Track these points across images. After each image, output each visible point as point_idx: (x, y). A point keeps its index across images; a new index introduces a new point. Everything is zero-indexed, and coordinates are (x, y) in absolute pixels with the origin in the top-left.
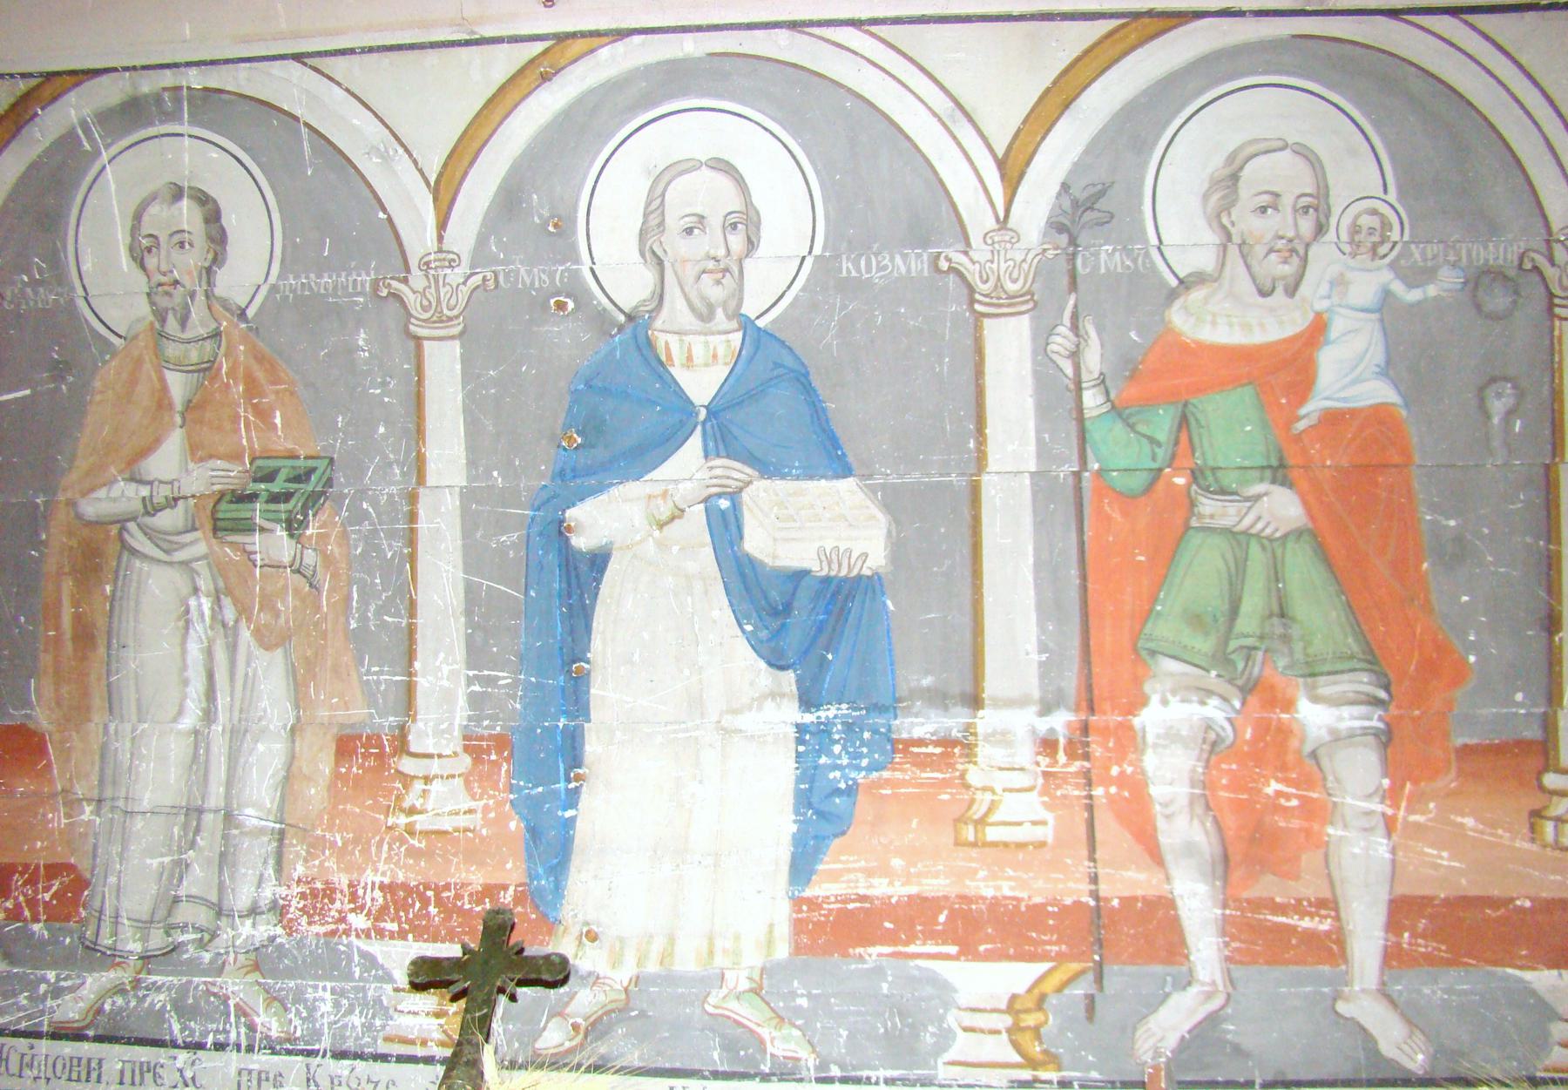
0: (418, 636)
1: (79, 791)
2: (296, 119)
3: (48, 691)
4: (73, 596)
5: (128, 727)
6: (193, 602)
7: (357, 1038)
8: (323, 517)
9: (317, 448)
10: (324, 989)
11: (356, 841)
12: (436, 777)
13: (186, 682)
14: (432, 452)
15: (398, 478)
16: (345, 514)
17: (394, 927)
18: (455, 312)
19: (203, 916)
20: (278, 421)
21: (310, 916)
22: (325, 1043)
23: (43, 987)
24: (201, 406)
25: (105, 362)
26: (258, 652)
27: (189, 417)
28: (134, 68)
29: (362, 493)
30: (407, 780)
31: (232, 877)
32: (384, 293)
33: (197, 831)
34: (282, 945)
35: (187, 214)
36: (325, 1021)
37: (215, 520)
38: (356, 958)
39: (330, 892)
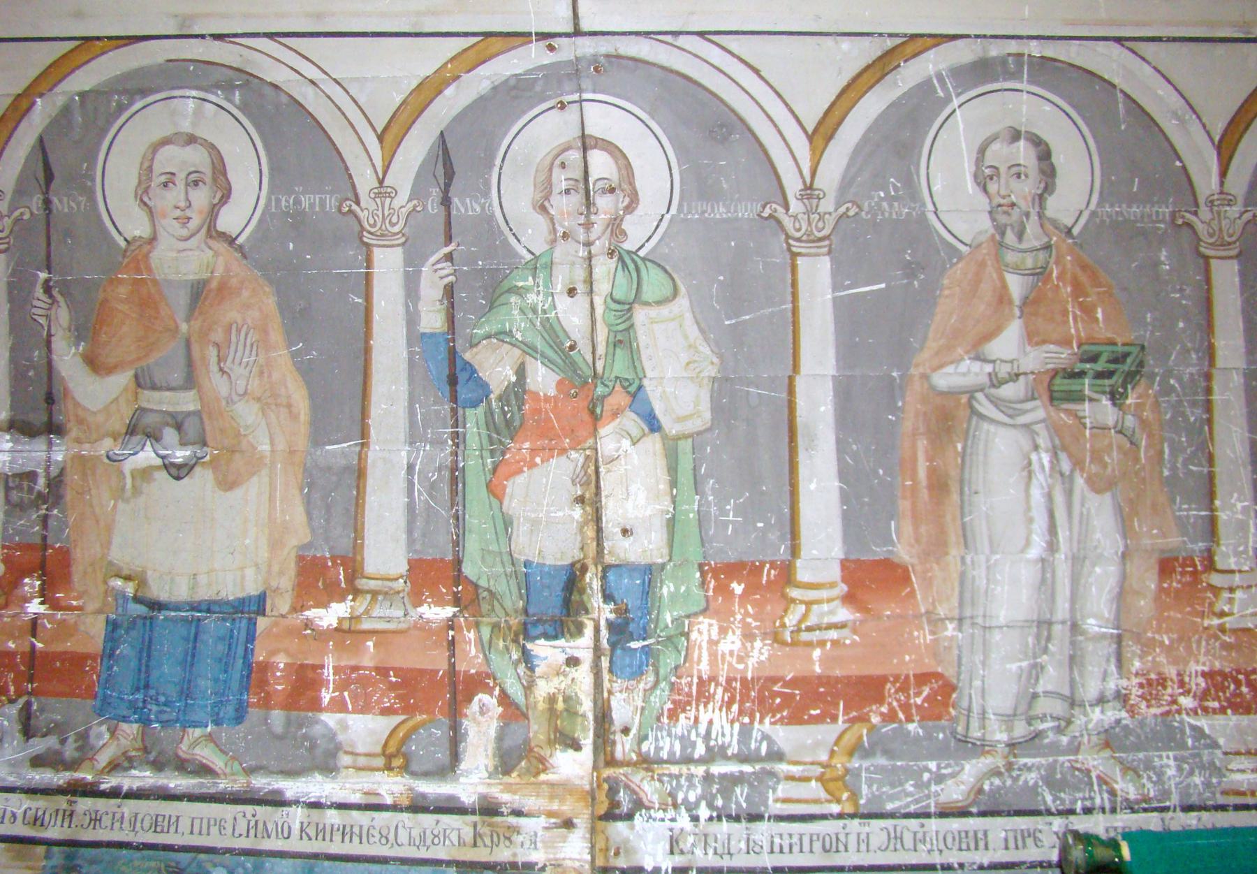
0: (1217, 481)
1: (941, 611)
2: (1114, 86)
3: (908, 528)
4: (926, 452)
5: (982, 558)
6: (1034, 457)
7: (1200, 794)
8: (1140, 389)
9: (1132, 337)
10: (1168, 757)
11: (1180, 639)
12: (1238, 587)
13: (1031, 520)
14: (1220, 343)
15: (1195, 361)
16: (1156, 387)
17: (1216, 704)
18: (1234, 239)
19: (1059, 708)
20: (1100, 315)
21: (1148, 701)
22: (1174, 799)
23: (926, 776)
24: (1036, 302)
25: (953, 265)
26: (1090, 495)
27: (1026, 310)
28: (985, 36)
29: (1168, 373)
30: (1216, 590)
31: (1081, 675)
32: (1180, 222)
33: (1049, 639)
34: (1127, 726)
35: (1023, 152)
36: (1172, 782)
37: (1051, 391)
38: (1188, 731)
39: (1162, 681)
